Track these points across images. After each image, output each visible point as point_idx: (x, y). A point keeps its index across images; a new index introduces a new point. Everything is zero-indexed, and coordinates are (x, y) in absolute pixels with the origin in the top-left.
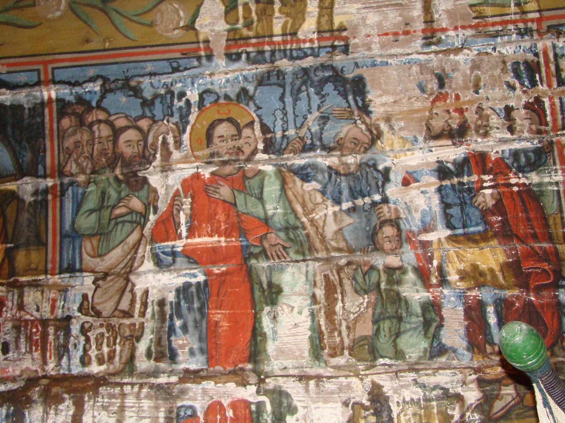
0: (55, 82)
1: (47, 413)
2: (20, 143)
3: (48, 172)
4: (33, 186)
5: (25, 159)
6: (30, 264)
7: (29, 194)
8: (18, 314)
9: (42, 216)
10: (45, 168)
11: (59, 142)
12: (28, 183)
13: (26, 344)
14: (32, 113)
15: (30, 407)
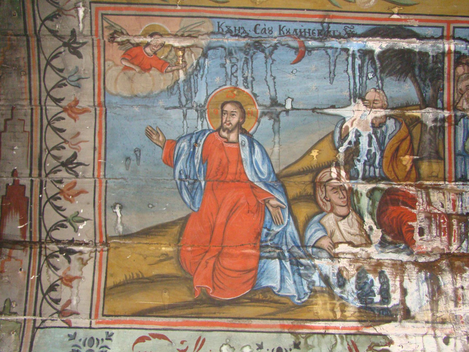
0: (454, 38)
1: (455, 279)
2: (424, 81)
3: (445, 106)
4: (433, 115)
5: (427, 94)
6: (432, 172)
7: (430, 121)
10: (442, 102)
11: (454, 84)
12: (429, 113)
15: (442, 274)
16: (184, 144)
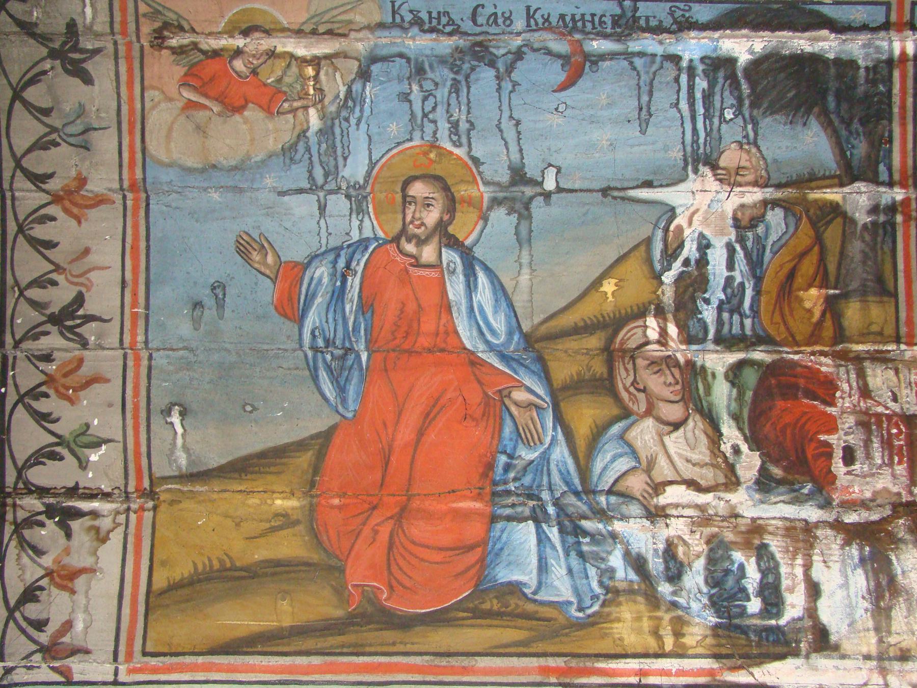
3: (896, 177)
4: (869, 199)
5: (855, 152)
6: (871, 324)
8: (862, 404)
9: (887, 249)
10: (890, 169)
13: (883, 452)
14: (871, 76)
15: (897, 548)
16: (322, 271)
